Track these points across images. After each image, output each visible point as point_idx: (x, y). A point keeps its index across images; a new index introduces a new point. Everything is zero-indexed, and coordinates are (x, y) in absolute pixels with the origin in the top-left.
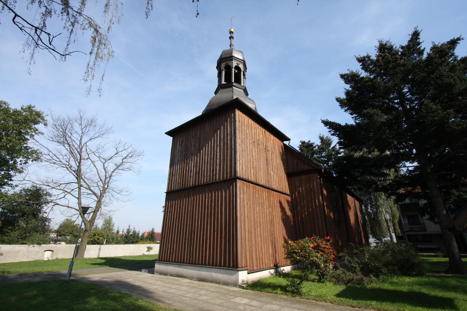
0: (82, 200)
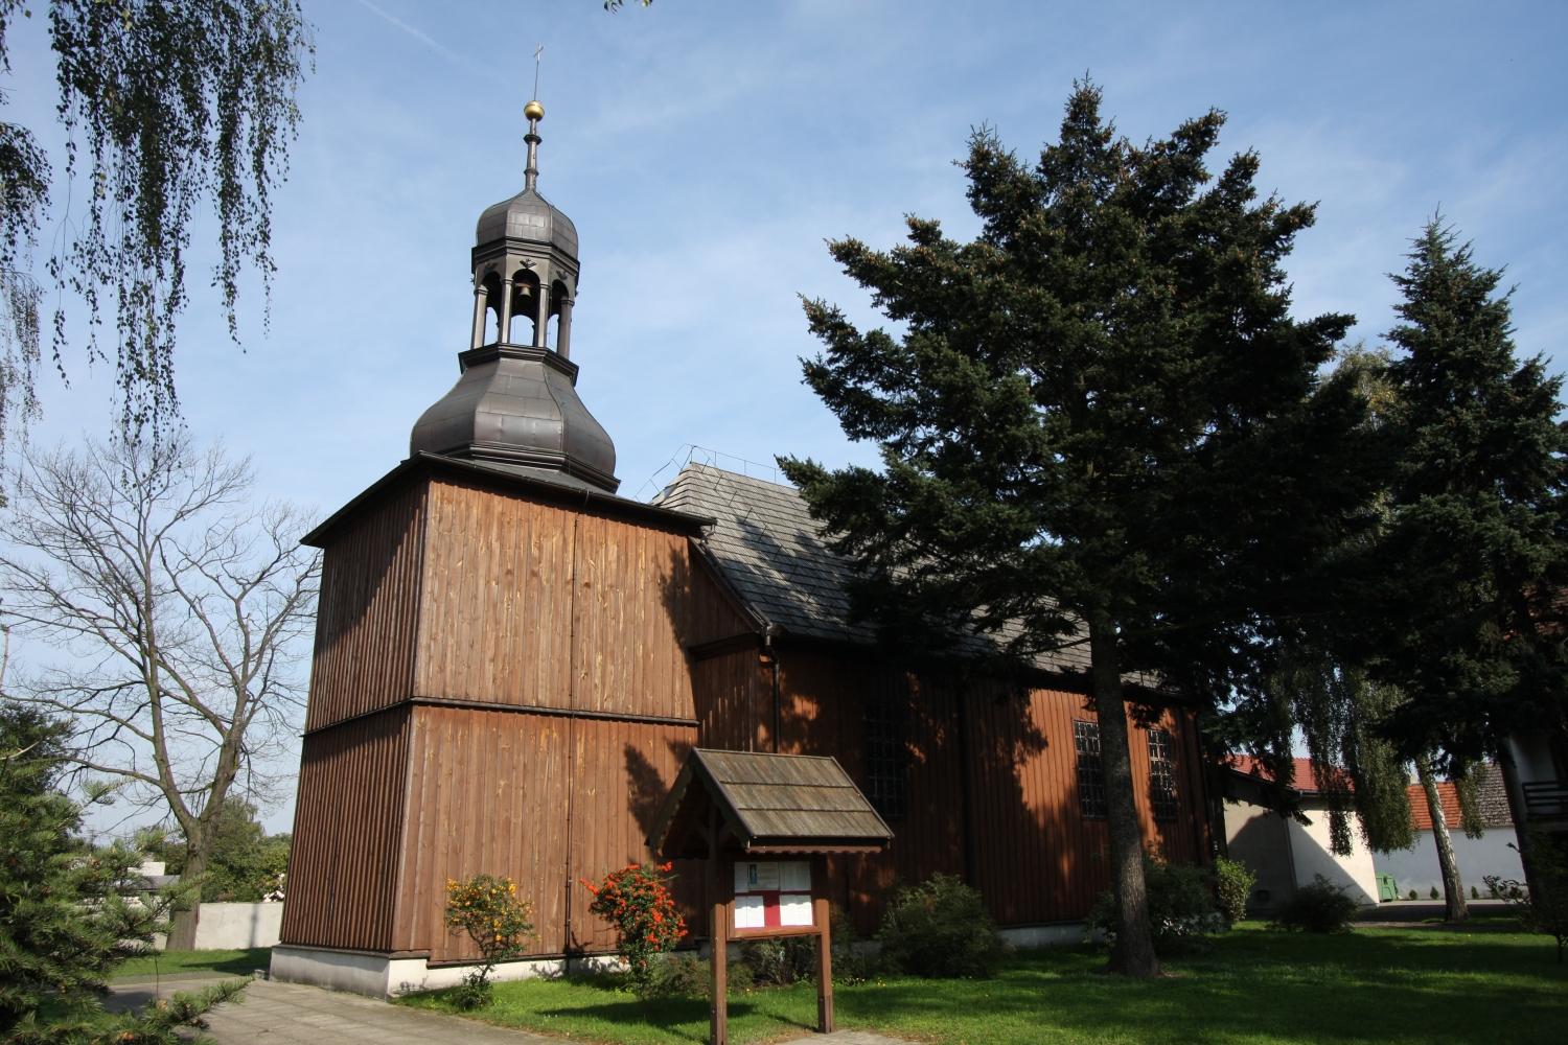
0: (168, 743)
